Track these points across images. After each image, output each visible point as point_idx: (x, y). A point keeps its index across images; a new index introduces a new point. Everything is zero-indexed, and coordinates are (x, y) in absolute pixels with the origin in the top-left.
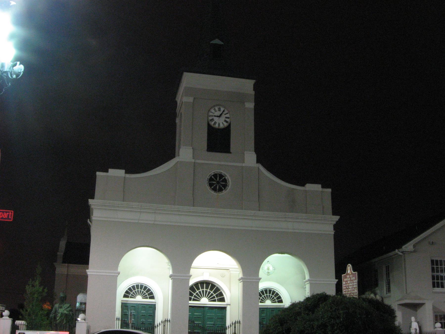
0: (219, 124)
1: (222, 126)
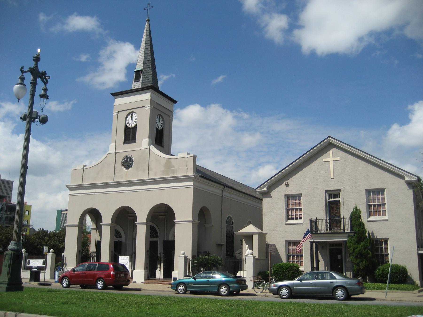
1: (160, 129)
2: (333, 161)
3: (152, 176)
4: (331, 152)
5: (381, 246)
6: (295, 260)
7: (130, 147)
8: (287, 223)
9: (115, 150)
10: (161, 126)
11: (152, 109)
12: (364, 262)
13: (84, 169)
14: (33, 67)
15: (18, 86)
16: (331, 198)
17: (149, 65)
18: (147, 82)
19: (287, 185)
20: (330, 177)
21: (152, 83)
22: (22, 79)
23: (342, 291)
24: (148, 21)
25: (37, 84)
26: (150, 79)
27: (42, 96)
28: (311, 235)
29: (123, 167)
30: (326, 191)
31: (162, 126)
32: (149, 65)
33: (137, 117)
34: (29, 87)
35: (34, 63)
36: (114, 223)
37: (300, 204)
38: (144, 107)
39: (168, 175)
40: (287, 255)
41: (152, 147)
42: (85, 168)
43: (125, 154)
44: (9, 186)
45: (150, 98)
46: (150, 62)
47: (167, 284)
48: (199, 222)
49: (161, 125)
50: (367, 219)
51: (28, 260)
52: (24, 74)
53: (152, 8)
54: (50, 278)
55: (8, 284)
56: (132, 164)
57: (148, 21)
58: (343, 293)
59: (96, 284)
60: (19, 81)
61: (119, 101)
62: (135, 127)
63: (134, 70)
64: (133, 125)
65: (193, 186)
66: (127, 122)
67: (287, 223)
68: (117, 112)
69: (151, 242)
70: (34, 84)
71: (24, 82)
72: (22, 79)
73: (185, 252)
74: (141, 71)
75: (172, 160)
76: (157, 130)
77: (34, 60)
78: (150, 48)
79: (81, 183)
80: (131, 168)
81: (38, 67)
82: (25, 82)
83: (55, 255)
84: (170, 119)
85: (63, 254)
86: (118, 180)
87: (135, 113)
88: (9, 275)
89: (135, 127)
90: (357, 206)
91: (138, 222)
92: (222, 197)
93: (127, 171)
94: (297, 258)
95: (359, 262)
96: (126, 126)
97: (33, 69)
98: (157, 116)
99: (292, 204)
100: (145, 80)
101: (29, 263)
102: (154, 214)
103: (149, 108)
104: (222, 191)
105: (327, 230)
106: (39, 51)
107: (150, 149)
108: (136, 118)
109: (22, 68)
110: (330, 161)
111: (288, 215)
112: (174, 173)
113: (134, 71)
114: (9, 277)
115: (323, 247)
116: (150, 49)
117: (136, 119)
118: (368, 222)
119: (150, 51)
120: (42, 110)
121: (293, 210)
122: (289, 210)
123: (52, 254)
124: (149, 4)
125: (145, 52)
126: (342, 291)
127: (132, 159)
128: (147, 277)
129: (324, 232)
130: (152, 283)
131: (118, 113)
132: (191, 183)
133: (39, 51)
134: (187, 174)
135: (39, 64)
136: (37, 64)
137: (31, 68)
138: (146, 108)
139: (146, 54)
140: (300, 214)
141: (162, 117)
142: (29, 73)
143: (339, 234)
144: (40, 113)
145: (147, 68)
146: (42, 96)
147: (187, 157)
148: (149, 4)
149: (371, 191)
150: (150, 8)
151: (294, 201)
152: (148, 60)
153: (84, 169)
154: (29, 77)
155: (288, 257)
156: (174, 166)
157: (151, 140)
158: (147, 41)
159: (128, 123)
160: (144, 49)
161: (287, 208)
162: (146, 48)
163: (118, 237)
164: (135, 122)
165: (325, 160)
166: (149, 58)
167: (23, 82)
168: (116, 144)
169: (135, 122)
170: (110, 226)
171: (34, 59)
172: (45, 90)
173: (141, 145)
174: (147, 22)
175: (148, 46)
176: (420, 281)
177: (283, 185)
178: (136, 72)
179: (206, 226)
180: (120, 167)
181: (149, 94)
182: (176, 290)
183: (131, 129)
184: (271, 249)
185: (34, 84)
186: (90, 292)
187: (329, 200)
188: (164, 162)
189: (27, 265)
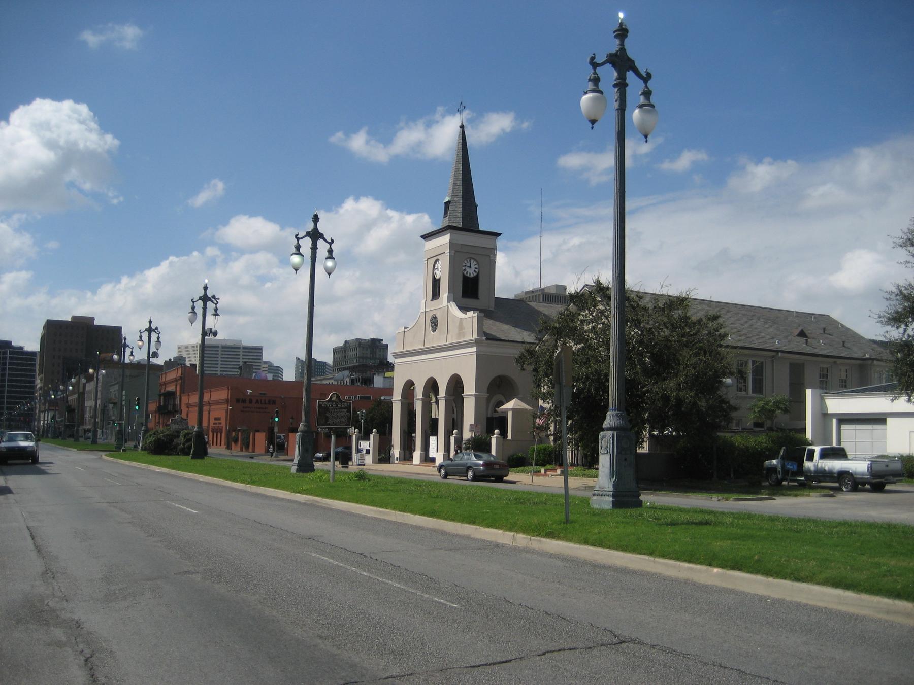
0: (467, 273)
1: (472, 276)
14: (614, 52)
15: (191, 314)
22: (596, 80)
25: (626, 85)
34: (612, 94)
35: (617, 41)
36: (451, 396)
38: (444, 253)
41: (451, 305)
42: (406, 330)
46: (461, 187)
48: (488, 395)
49: (475, 271)
52: (598, 70)
55: (614, 496)
59: (467, 473)
60: (590, 86)
66: (435, 272)
68: (426, 259)
70: (621, 85)
71: (599, 87)
72: (596, 80)
77: (616, 37)
79: (423, 347)
81: (625, 50)
82: (601, 86)
85: (414, 435)
88: (613, 477)
89: (439, 279)
91: (464, 394)
97: (616, 55)
106: (621, 15)
109: (593, 59)
114: (614, 482)
119: (461, 172)
123: (496, 437)
124: (461, 103)
132: (474, 349)
133: (621, 15)
135: (627, 42)
136: (622, 44)
137: (610, 54)
139: (457, 177)
141: (475, 260)
142: (608, 66)
153: (404, 332)
154: (609, 74)
167: (598, 87)
170: (474, 398)
171: (616, 33)
175: (459, 165)
178: (445, 203)
181: (449, 235)
185: (621, 85)
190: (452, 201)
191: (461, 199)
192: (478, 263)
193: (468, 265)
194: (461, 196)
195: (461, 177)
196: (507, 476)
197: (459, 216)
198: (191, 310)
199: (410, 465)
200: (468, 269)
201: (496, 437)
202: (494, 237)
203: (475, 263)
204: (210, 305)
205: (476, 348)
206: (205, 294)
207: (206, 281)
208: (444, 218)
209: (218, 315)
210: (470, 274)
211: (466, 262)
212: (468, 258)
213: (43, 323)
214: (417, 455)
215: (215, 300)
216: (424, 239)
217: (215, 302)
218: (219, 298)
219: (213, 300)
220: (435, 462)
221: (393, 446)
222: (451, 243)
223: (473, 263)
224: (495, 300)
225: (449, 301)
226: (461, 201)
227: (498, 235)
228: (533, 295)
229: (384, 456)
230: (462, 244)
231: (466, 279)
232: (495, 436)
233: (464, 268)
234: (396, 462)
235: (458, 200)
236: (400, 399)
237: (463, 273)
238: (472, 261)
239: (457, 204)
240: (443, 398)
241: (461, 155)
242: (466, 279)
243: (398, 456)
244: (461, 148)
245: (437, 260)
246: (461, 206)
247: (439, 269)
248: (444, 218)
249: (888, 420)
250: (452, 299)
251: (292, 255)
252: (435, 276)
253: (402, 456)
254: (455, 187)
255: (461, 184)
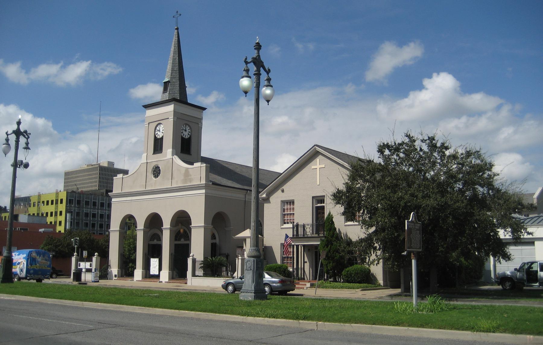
0: (184, 135)
1: (187, 137)
2: (320, 168)
3: (174, 185)
4: (318, 160)
5: (316, 250)
6: (289, 262)
7: (158, 156)
8: (282, 227)
9: (147, 160)
10: (188, 135)
11: (176, 120)
12: (331, 264)
13: (123, 178)
16: (319, 204)
17: (176, 75)
18: (173, 93)
19: (283, 191)
20: (317, 184)
21: (179, 93)
23: (268, 289)
24: (177, 29)
26: (177, 89)
27: (25, 148)
28: (291, 239)
29: (153, 176)
30: (313, 197)
31: (190, 134)
32: (176, 75)
33: (163, 128)
37: (293, 209)
38: (169, 118)
39: (186, 184)
40: (283, 257)
41: (175, 157)
43: (154, 164)
44: (105, 180)
45: (173, 110)
46: (178, 71)
47: (183, 283)
49: (188, 134)
50: (345, 223)
51: (79, 263)
53: (180, 16)
54: (192, 275)
56: (159, 173)
57: (177, 29)
58: (268, 291)
61: (150, 112)
62: (162, 138)
63: (163, 80)
64: (161, 136)
65: (204, 194)
66: (156, 133)
67: (282, 227)
68: (148, 123)
69: (176, 245)
73: (194, 255)
74: (169, 82)
75: (190, 170)
76: (183, 139)
78: (178, 58)
79: (120, 192)
80: (159, 177)
83: (99, 258)
84: (199, 127)
86: (149, 188)
87: (162, 124)
89: (162, 138)
90: (331, 211)
91: (164, 227)
92: (245, 201)
93: (156, 180)
94: (291, 259)
95: (328, 264)
96: (155, 137)
98: (184, 126)
99: (287, 209)
100: (172, 91)
101: (80, 266)
102: (178, 219)
103: (173, 119)
104: (246, 195)
105: (313, 234)
107: (173, 159)
108: (163, 129)
110: (317, 168)
111: (284, 220)
112: (191, 182)
113: (163, 82)
115: (309, 250)
116: (177, 59)
117: (163, 130)
118: (345, 226)
119: (178, 61)
120: (26, 158)
121: (288, 214)
122: (285, 215)
124: (177, 12)
125: (173, 63)
126: (268, 289)
127: (160, 168)
128: (171, 277)
129: (310, 236)
130: (173, 283)
131: (149, 125)
132: (203, 191)
134: (200, 182)
135: (21, 127)
138: (170, 120)
139: (174, 64)
140: (291, 218)
141: (189, 126)
143: (298, 239)
144: (24, 161)
145: (174, 78)
146: (25, 148)
147: (201, 167)
148: (177, 12)
149: (283, 207)
150: (176, 16)
151: (289, 207)
152: (176, 70)
153: (123, 178)
155: (283, 259)
156: (191, 175)
157: (175, 150)
158: (175, 51)
159: (157, 134)
160: (172, 59)
161: (283, 213)
162: (174, 57)
163: (158, 241)
164: (162, 133)
165: (313, 167)
166: (177, 68)
168: (147, 154)
169: (162, 133)
170: (143, 231)
172: (27, 144)
173: (166, 156)
174: (176, 30)
175: (176, 56)
176: (383, 281)
177: (280, 191)
178: (164, 83)
179: (226, 229)
180: (151, 176)
181: (173, 106)
182: (226, 290)
183: (160, 140)
184: (239, 252)
186: (143, 290)
187: (316, 206)
188: (183, 171)
189: (79, 267)
190: (171, 82)
191: (178, 80)
192: (191, 128)
193: (184, 129)
194: (178, 78)
195: (177, 65)
196: (293, 290)
197: (177, 93)
198: (5, 142)
199: (132, 280)
200: (184, 132)
201: (96, 257)
202: (201, 110)
203: (189, 128)
204: (22, 140)
205: (204, 190)
206: (18, 128)
207: (20, 117)
208: (163, 93)
209: (29, 149)
210: (185, 135)
211: (183, 127)
212: (184, 124)
213: (262, 74)
214: (138, 273)
215: (27, 135)
216: (145, 108)
217: (27, 137)
218: (30, 134)
219: (25, 134)
220: (160, 278)
221: (110, 266)
222: (175, 111)
223: (188, 128)
224: (201, 158)
225: (173, 155)
226: (178, 82)
227: (204, 109)
228: (92, 167)
229: (104, 273)
230: (181, 113)
231: (183, 139)
232: (75, 256)
233: (182, 131)
234: (114, 278)
235: (176, 81)
236: (119, 229)
237: (182, 136)
238: (187, 126)
239: (175, 84)
240: (202, 226)
241: (177, 49)
242: (183, 139)
243: (117, 274)
244: (177, 44)
245: (160, 124)
246: (178, 86)
247: (161, 131)
248: (163, 93)
249: (536, 243)
250: (175, 152)
251: (243, 77)
252: (157, 136)
253: (120, 274)
254: (173, 71)
255: (178, 69)
